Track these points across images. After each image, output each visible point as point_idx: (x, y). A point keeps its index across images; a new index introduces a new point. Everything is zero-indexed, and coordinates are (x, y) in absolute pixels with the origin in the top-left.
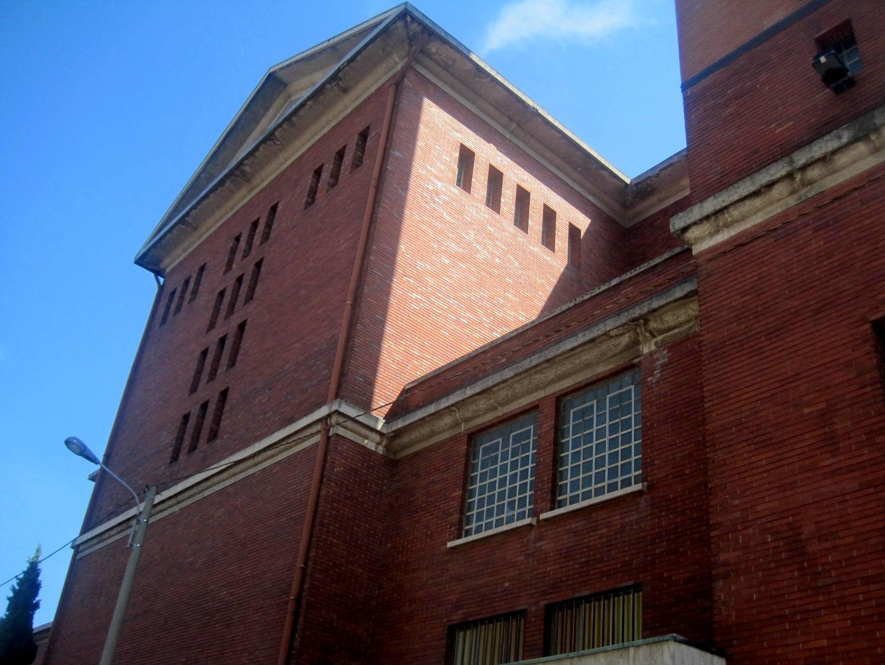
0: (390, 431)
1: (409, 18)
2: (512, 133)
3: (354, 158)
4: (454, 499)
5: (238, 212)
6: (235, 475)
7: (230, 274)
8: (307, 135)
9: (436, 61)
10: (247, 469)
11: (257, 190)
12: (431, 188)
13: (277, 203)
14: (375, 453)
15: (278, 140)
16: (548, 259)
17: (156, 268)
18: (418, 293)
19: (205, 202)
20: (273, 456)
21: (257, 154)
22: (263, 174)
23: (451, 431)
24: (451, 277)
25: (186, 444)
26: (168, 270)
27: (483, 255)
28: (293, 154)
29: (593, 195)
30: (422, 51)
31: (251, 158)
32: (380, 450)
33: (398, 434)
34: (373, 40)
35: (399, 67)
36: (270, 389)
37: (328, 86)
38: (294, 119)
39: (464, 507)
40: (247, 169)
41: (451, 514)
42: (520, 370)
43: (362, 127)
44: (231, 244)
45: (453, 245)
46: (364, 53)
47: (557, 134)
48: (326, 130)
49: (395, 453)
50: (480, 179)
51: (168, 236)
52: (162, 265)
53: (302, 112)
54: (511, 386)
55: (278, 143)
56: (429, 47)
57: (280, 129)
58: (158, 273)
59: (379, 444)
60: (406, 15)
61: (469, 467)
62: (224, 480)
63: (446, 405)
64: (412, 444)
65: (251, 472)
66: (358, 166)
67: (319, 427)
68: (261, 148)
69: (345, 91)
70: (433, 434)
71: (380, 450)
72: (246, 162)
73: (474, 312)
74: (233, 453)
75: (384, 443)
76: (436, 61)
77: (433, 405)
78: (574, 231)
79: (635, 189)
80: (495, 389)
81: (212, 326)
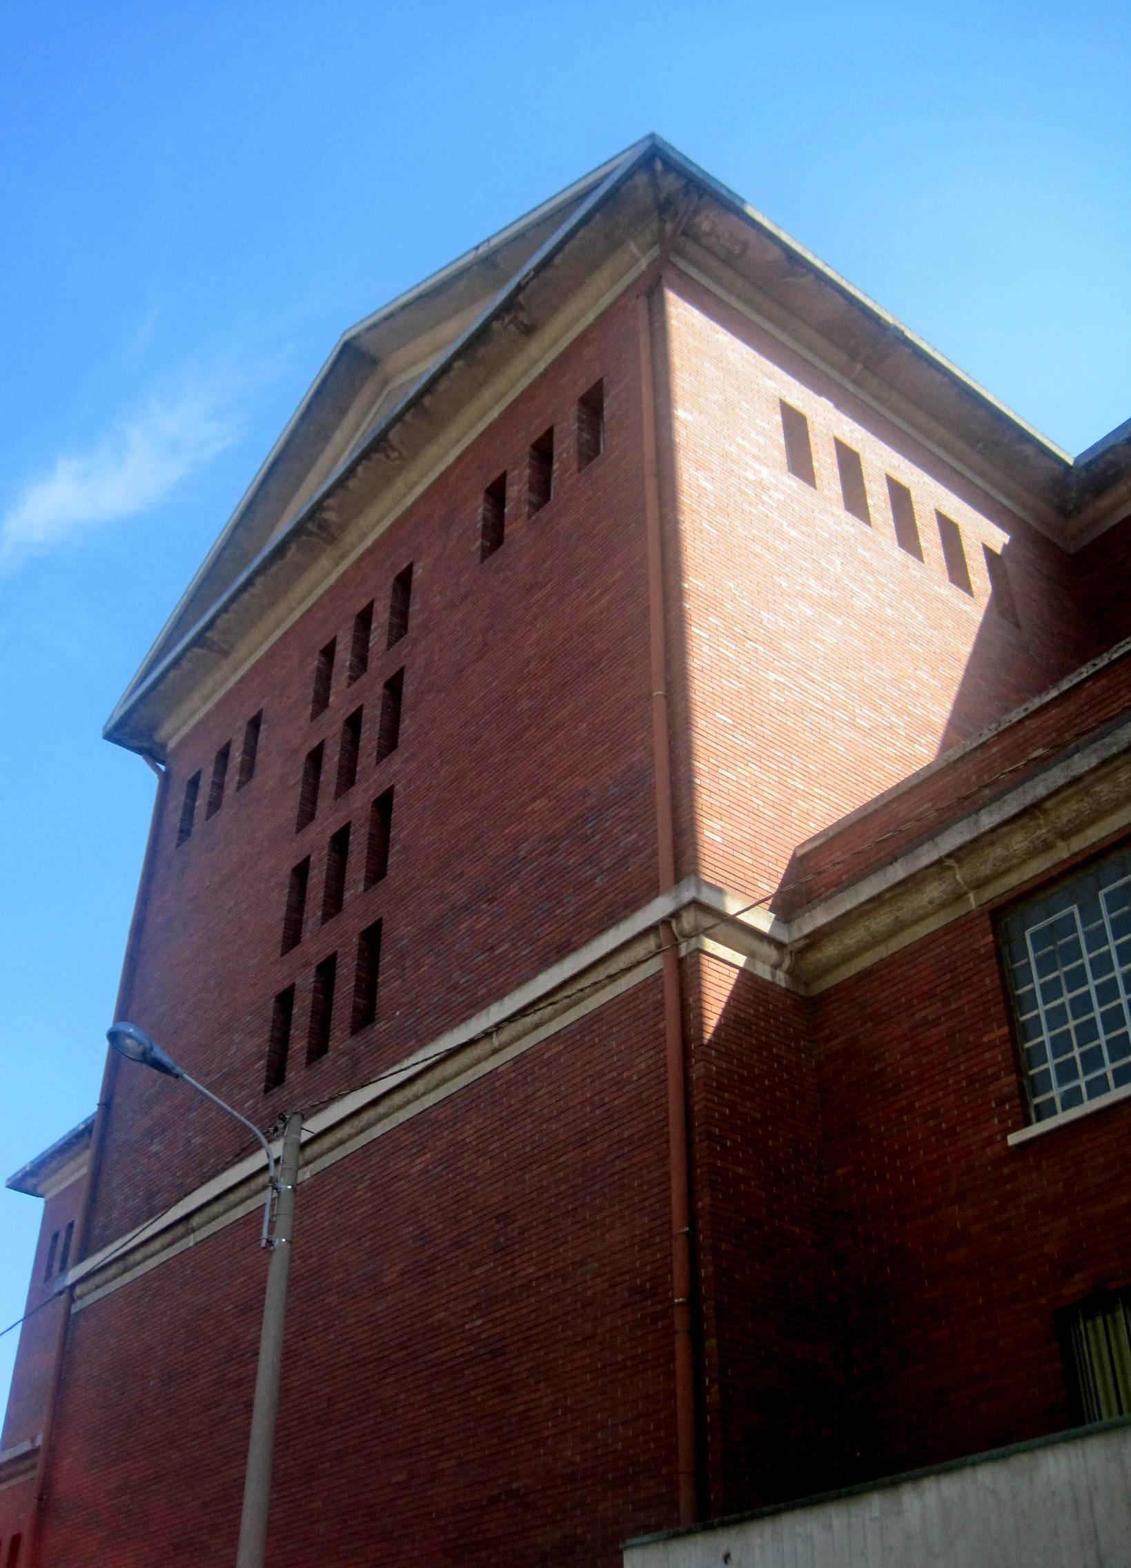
0: (796, 935)
1: (659, 166)
2: (856, 382)
3: (580, 444)
4: (991, 1046)
5: (316, 604)
6: (444, 1081)
7: (327, 715)
8: (453, 431)
9: (708, 249)
10: (477, 1062)
11: (354, 555)
12: (752, 477)
13: (410, 567)
14: (772, 984)
15: (393, 449)
16: (966, 608)
17: (145, 744)
18: (775, 671)
19: (246, 596)
20: (537, 1026)
21: (352, 483)
22: (363, 522)
23: (942, 914)
24: (822, 642)
25: (299, 1042)
26: (172, 744)
27: (863, 602)
28: (423, 475)
29: (1007, 495)
30: (684, 233)
31: (340, 493)
32: (781, 979)
33: (815, 939)
34: (584, 221)
35: (643, 265)
36: (491, 901)
37: (496, 325)
38: (427, 401)
39: (1020, 1060)
40: (330, 516)
41: (995, 1077)
42: (1114, 750)
43: (582, 387)
44: (315, 662)
45: (812, 582)
46: (568, 248)
47: (938, 377)
48: (495, 414)
49: (807, 984)
50: (825, 463)
51: (172, 674)
52: (160, 736)
53: (443, 386)
54: (1086, 791)
55: (394, 455)
56: (697, 220)
57: (398, 426)
58: (153, 753)
59: (776, 966)
60: (654, 158)
61: (1007, 980)
62: (417, 1097)
63: (935, 856)
64: (832, 967)
65: (486, 1067)
66: (590, 459)
67: (651, 943)
68: (360, 469)
69: (529, 331)
70: (900, 926)
71: (781, 979)
72: (330, 501)
73: (875, 708)
74: (422, 1043)
75: (787, 963)
76: (708, 249)
77: (897, 865)
78: (991, 557)
79: (1084, 474)
80: (1048, 804)
81: (307, 816)
